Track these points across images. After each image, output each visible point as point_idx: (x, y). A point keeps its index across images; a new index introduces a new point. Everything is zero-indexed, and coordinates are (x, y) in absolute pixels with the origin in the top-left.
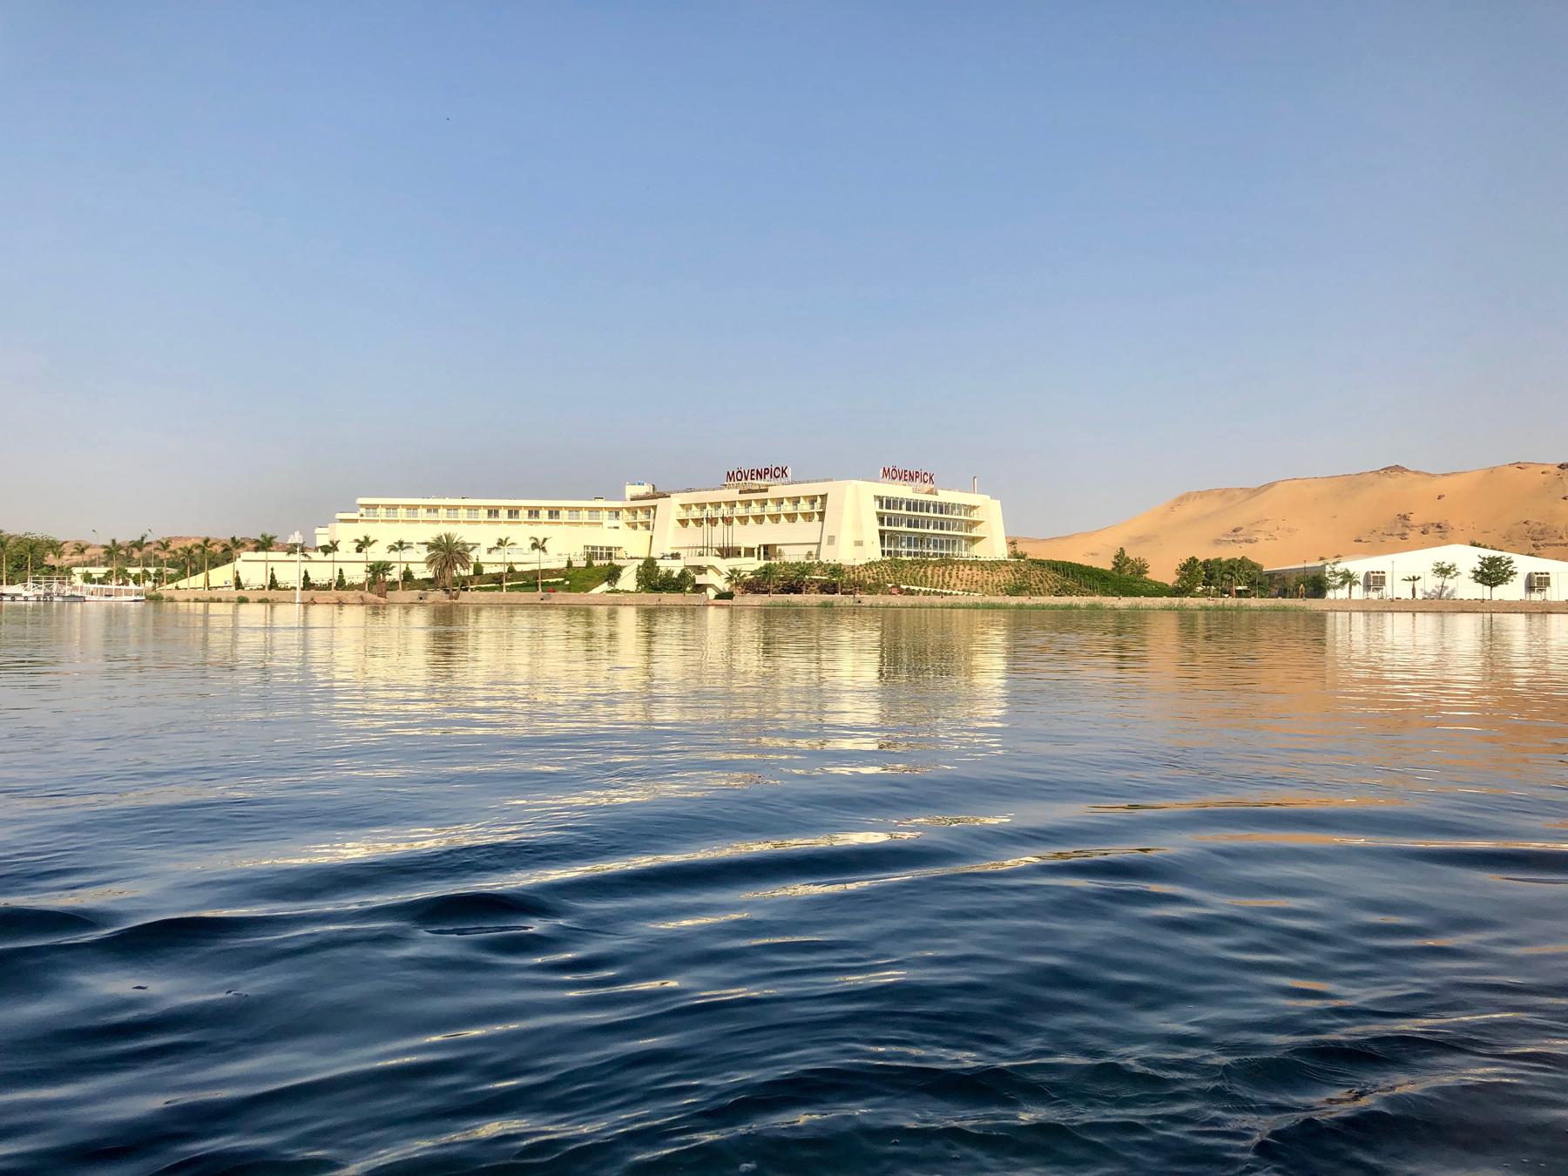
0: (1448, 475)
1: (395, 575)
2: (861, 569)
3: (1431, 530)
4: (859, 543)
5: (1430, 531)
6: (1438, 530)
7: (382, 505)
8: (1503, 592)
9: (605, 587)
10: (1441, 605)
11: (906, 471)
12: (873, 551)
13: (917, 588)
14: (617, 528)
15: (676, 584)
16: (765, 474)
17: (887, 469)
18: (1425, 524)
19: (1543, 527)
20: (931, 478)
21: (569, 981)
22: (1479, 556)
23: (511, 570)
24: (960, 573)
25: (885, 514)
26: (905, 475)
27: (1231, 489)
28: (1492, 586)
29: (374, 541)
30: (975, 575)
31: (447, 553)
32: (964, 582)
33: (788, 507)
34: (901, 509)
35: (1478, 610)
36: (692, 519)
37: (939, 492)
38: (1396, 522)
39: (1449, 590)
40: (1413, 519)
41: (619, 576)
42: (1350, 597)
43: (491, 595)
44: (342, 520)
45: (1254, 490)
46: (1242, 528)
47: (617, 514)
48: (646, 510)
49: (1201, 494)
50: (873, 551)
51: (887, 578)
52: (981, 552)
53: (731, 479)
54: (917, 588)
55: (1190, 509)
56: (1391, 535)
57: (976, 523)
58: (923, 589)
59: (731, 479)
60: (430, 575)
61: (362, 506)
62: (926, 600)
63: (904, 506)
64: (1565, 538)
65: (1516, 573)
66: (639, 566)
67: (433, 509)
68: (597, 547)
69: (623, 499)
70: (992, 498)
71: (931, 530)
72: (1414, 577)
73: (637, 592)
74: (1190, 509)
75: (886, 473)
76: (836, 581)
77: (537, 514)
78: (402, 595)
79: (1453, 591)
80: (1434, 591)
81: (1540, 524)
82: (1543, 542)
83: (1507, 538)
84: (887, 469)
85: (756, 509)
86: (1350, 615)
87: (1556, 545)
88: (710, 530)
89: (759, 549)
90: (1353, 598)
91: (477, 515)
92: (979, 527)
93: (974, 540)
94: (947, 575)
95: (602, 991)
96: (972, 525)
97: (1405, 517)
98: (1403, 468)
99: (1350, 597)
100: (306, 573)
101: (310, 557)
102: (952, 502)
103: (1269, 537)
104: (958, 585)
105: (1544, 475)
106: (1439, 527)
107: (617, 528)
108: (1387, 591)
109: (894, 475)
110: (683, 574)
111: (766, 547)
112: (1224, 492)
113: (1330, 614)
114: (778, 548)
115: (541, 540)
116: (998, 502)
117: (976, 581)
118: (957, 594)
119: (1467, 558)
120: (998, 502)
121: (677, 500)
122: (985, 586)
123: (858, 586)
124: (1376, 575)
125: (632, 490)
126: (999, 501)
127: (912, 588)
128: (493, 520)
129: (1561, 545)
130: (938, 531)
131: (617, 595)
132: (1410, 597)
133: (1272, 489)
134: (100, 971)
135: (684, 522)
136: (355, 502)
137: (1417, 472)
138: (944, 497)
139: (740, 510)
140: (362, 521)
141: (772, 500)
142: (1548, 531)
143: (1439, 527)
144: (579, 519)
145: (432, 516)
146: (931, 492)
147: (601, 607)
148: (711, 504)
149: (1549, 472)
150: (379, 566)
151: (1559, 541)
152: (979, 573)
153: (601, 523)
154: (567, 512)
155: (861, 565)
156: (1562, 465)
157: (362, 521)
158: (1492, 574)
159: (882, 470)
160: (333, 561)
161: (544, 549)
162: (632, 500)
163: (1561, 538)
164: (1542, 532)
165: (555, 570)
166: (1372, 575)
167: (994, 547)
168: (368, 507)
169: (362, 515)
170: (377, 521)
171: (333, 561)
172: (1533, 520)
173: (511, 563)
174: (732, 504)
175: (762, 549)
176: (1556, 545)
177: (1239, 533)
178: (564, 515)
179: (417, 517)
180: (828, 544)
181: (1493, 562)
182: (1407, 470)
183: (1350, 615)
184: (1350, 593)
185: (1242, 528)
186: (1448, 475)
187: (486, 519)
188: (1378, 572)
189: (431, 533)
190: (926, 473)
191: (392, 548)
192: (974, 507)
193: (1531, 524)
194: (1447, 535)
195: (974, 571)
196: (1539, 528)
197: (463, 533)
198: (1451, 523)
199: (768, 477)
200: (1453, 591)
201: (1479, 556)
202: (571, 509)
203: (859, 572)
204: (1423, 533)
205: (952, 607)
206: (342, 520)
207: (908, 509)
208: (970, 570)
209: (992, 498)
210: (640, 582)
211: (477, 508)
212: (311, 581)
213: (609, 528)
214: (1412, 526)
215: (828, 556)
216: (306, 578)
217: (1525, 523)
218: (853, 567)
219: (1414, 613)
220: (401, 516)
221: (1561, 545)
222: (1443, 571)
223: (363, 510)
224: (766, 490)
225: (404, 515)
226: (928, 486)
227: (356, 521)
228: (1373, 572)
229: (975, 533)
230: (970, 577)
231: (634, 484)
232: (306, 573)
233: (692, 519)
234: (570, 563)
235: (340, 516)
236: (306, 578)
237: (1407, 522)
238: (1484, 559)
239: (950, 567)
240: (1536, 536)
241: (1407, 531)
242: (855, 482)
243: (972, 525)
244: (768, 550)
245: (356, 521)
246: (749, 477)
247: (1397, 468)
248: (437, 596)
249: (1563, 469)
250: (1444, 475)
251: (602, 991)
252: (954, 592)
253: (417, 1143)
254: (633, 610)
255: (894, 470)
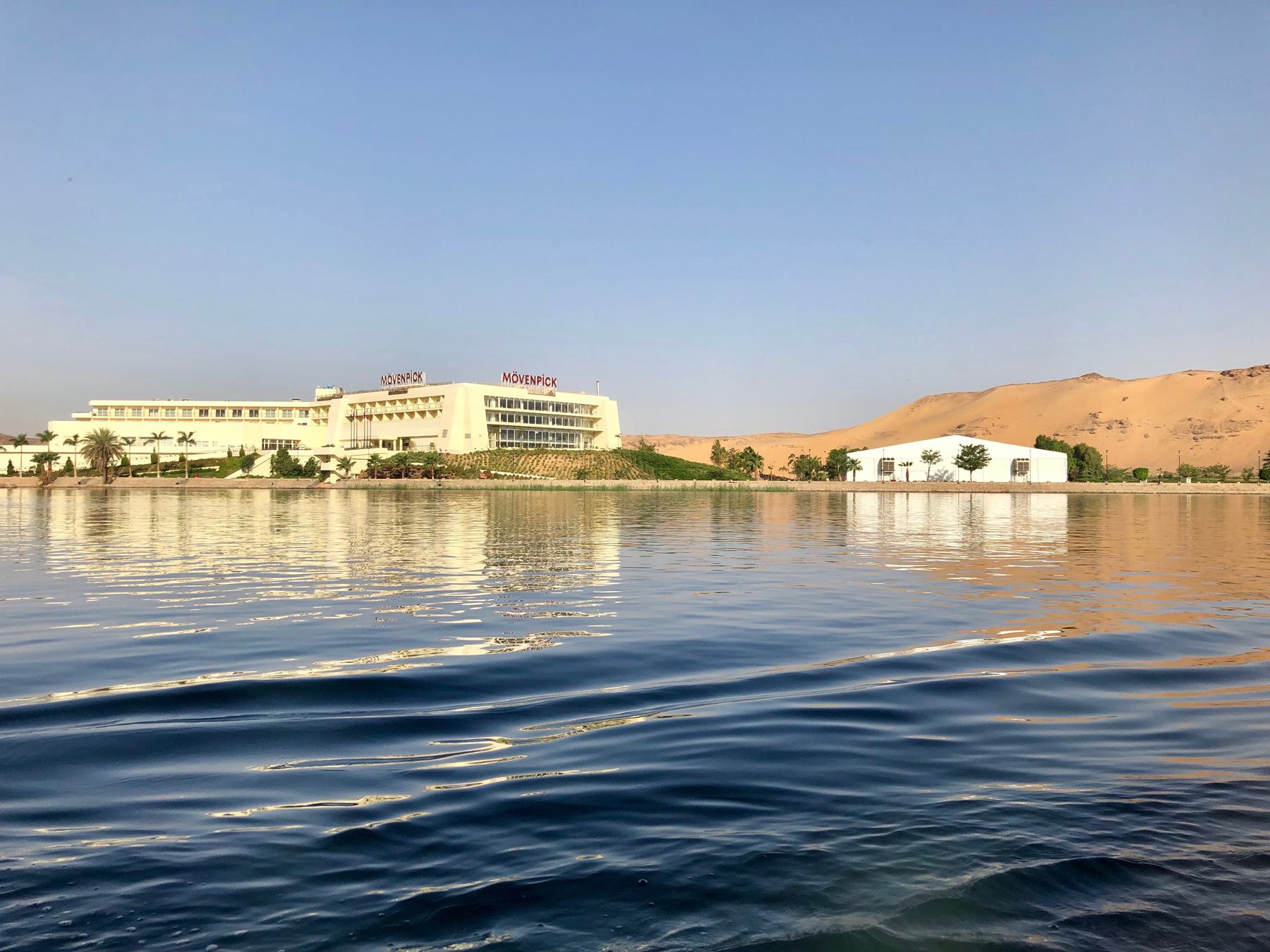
0: (1133, 380)
1: (57, 466)
2: (464, 457)
3: (1115, 425)
4: (468, 436)
5: (1113, 426)
6: (1120, 425)
7: (279, 408)
8: (979, 476)
9: (239, 473)
10: (938, 487)
11: (527, 376)
12: (482, 442)
13: (503, 473)
14: (305, 424)
15: (309, 471)
16: (407, 378)
17: (507, 375)
18: (1111, 421)
19: (1202, 423)
20: (553, 382)
21: (484, 779)
22: (960, 445)
23: (182, 460)
24: (546, 461)
25: (498, 411)
26: (527, 380)
27: (962, 393)
28: (971, 469)
29: (55, 436)
30: (558, 463)
31: (102, 447)
32: (546, 469)
33: (421, 406)
34: (519, 407)
35: (949, 490)
36: (397, 414)
37: (556, 393)
38: (1087, 419)
39: (949, 473)
40: (1102, 418)
41: (253, 463)
42: (854, 480)
43: (137, 481)
44: (78, 419)
45: (979, 394)
46: (964, 425)
47: (307, 412)
48: (324, 408)
49: (938, 398)
50: (482, 442)
51: (483, 465)
52: (599, 444)
53: (507, 380)
54: (503, 473)
55: (926, 410)
56: (1083, 430)
57: (595, 420)
58: (508, 474)
59: (507, 380)
60: (88, 466)
61: (95, 407)
62: (507, 483)
63: (522, 405)
64: (1219, 432)
65: (991, 459)
66: (273, 456)
67: (154, 409)
68: (282, 440)
69: (312, 400)
70: (610, 399)
71: (550, 425)
72: (907, 463)
73: (271, 477)
74: (926, 410)
75: (506, 377)
76: (435, 466)
77: (240, 412)
78: (66, 481)
79: (952, 475)
80: (936, 474)
81: (1200, 421)
82: (1201, 435)
83: (1174, 432)
84: (507, 375)
85: (400, 408)
86: (854, 495)
87: (1212, 438)
88: (369, 425)
89: (398, 441)
90: (911, 479)
91: (122, 414)
92: (599, 422)
93: (595, 434)
94: (535, 463)
95: (1154, 800)
96: (592, 421)
97: (1094, 416)
98: (1098, 375)
99: (854, 480)
100: (10, 462)
101: (5, 449)
102: (565, 401)
103: (986, 432)
104: (541, 471)
105: (1209, 381)
106: (1121, 423)
107: (305, 424)
108: (899, 474)
109: (515, 379)
110: (311, 462)
111: (404, 439)
112: (956, 395)
113: (850, 496)
114: (411, 439)
115: (188, 434)
116: (615, 402)
117: (557, 468)
118: (535, 479)
119: (950, 447)
120: (615, 402)
121: (347, 400)
122: (563, 472)
123: (457, 472)
124: (1021, 461)
125: (321, 392)
126: (615, 402)
127: (499, 473)
128: (220, 418)
129: (1216, 437)
130: (556, 426)
131: (1221, 487)
132: (905, 480)
133: (993, 392)
134: (169, 775)
135: (351, 418)
136: (88, 403)
137: (1109, 379)
138: (561, 397)
139: (389, 408)
140: (95, 419)
141: (411, 400)
142: (1206, 426)
143: (1121, 423)
144: (141, 416)
145: (153, 416)
146: (551, 394)
147: (235, 490)
148: (369, 403)
149: (1213, 378)
150: (42, 456)
151: (1214, 435)
152: (563, 461)
153: (292, 420)
154: (264, 411)
155: (465, 455)
156: (1224, 372)
157: (95, 419)
158: (972, 459)
159: (502, 376)
160: (21, 453)
161: (192, 441)
162: (318, 400)
163: (1216, 432)
164: (1201, 427)
165: (218, 459)
166: (1018, 461)
167: (610, 437)
168: (100, 408)
169: (95, 415)
170: (107, 419)
171: (21, 453)
172: (1196, 417)
173: (182, 454)
174: (382, 403)
175: (401, 441)
176: (1212, 438)
177: (961, 429)
178: (262, 413)
179: (141, 416)
180: (443, 437)
181: (969, 450)
182: (1102, 377)
183: (854, 495)
184: (854, 476)
185: (964, 425)
186: (1133, 380)
187: (197, 416)
188: (1023, 459)
189: (85, 429)
190: (415, 373)
191: (68, 442)
192: (595, 407)
193: (1193, 420)
194: (1127, 430)
195: (559, 459)
196: (1199, 424)
197: (119, 430)
198: (1131, 421)
199: (540, 384)
200: (952, 475)
201: (960, 445)
202: (268, 409)
203: (461, 461)
204: (1108, 428)
205: (756, 491)
206: (78, 419)
207: (525, 408)
208: (556, 458)
209: (610, 399)
210: (273, 469)
211: (190, 408)
212: (15, 469)
213: (299, 424)
214: (1100, 423)
215: (442, 446)
216: (10, 466)
217: (1189, 420)
218: (457, 456)
219: (908, 493)
220: (144, 416)
221: (1216, 437)
222: (929, 458)
223: (96, 411)
224: (406, 392)
225: (164, 414)
226: (547, 390)
227: (89, 419)
228: (1019, 459)
229: (595, 429)
230: (554, 464)
231: (325, 388)
232: (10, 462)
233: (397, 414)
234: (230, 453)
235: (75, 415)
236: (10, 466)
237: (1095, 419)
238: (964, 447)
239: (541, 455)
240: (1196, 430)
241: (1096, 427)
242: (466, 385)
243: (592, 421)
244: (406, 442)
245: (89, 419)
246: (396, 382)
247: (1093, 375)
248: (97, 481)
249: (1225, 375)
250: (1130, 381)
251: (1154, 800)
252: (533, 477)
253: (421, 889)
254: (268, 493)
255: (514, 375)
